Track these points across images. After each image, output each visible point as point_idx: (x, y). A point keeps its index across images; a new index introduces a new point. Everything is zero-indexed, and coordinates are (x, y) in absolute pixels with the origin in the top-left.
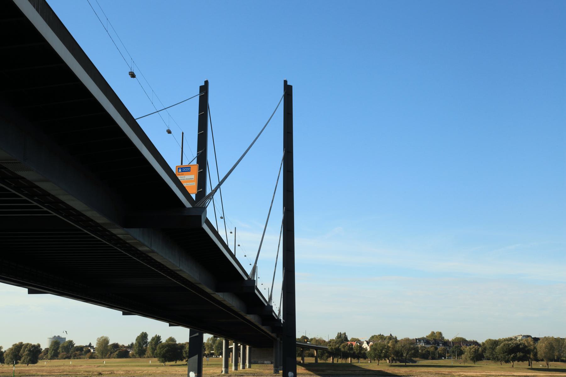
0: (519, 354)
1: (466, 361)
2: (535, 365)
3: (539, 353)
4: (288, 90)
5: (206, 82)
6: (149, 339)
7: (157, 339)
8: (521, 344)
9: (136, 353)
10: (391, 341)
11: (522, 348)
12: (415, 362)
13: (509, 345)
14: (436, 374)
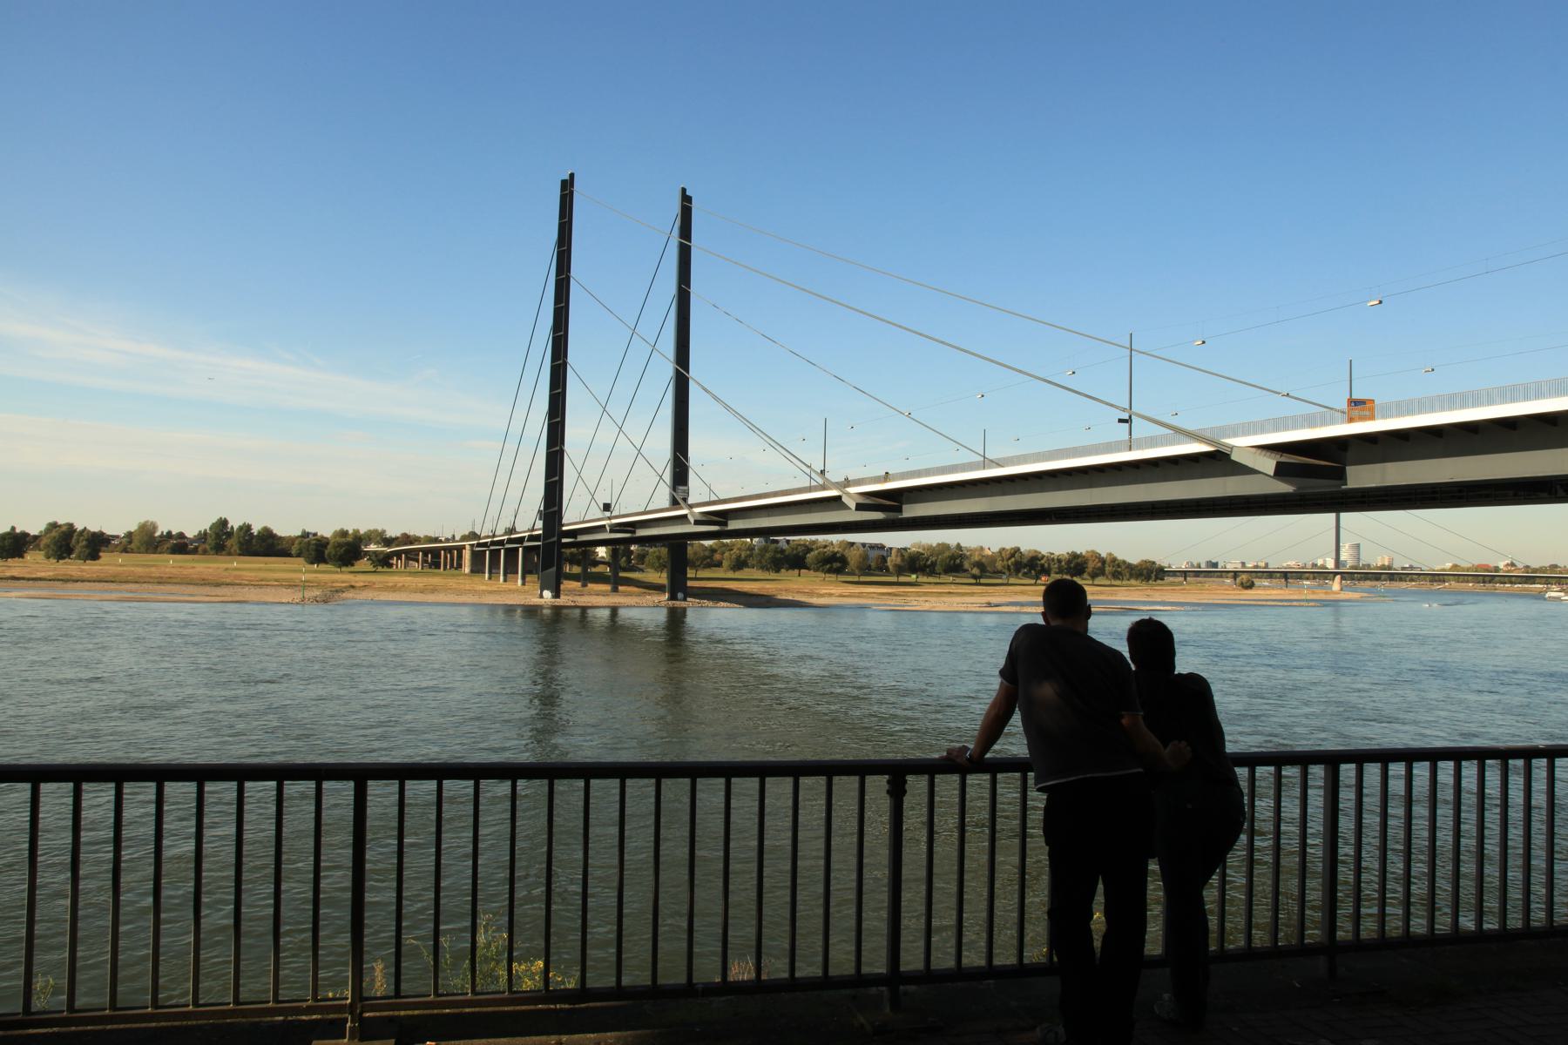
4: (686, 199)
5: (572, 176)
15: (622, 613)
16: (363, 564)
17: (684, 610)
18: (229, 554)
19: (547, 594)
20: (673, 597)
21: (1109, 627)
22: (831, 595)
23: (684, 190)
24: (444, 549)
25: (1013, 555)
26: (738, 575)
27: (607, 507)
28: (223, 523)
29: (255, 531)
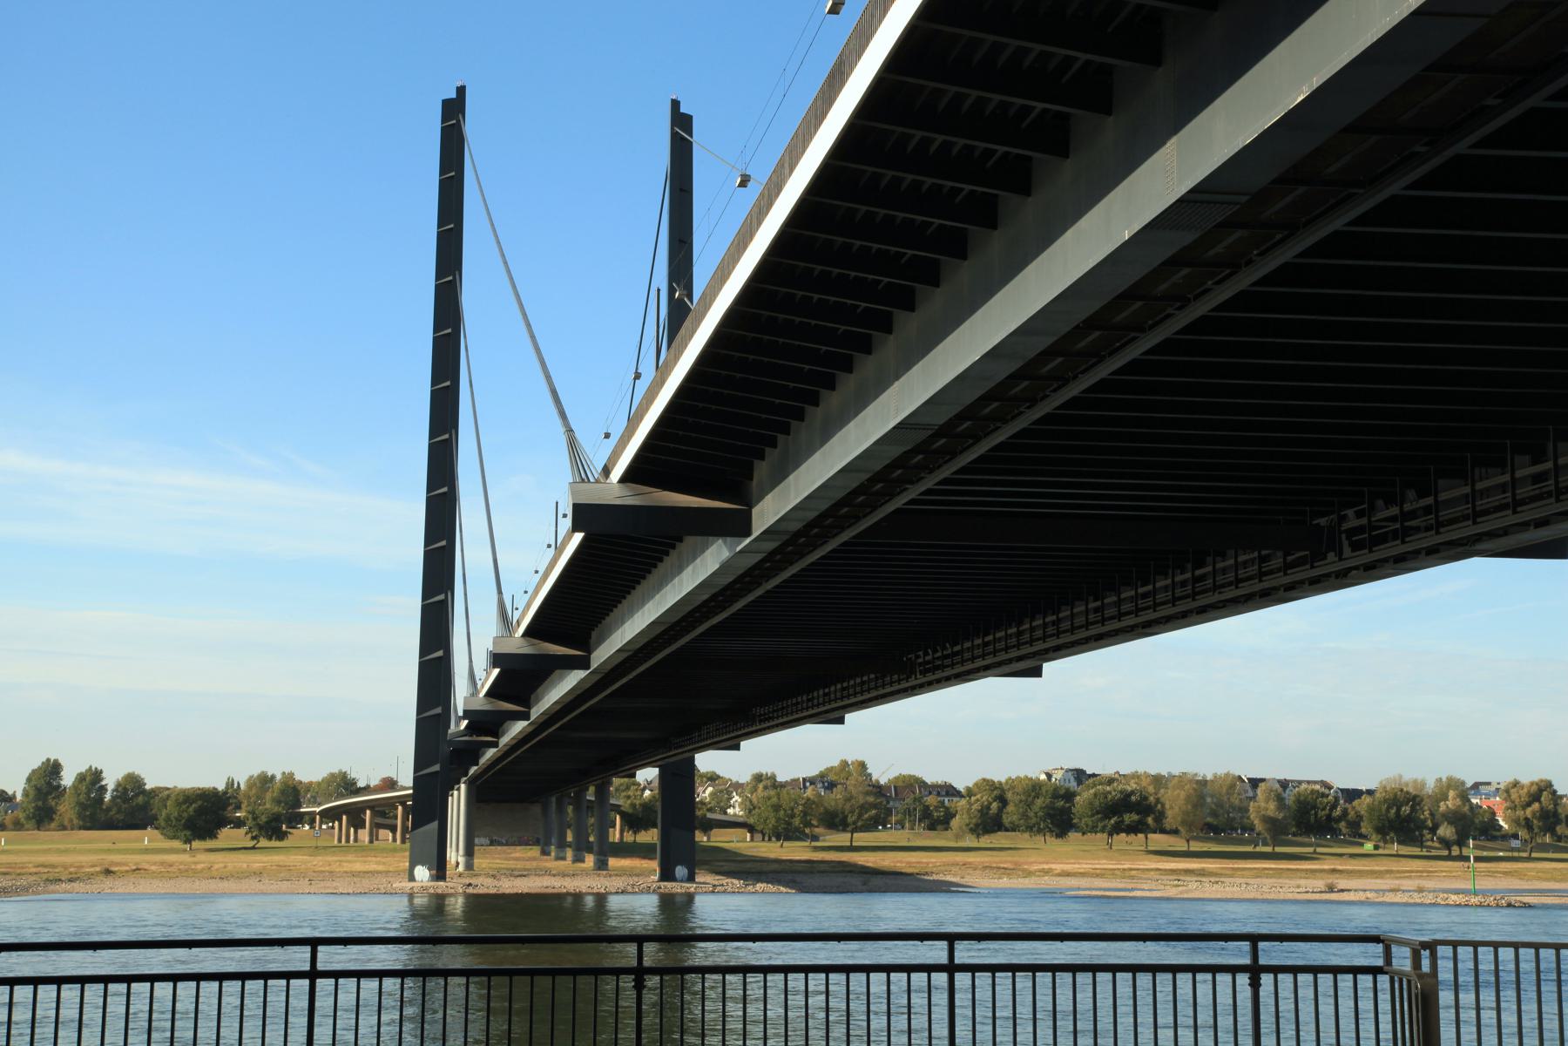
0: (1131, 818)
1: (958, 837)
2: (1158, 840)
3: (1169, 813)
4: (681, 122)
5: (461, 91)
6: (68, 779)
7: (93, 778)
8: (1132, 793)
9: (28, 818)
10: (761, 786)
11: (1138, 803)
12: (815, 838)
13: (1106, 794)
14: (985, 868)
15: (614, 902)
16: (227, 835)
17: (690, 898)
18: (64, 828)
19: (422, 873)
20: (667, 875)
21: (590, 860)
22: (1046, 872)
23: (675, 104)
24: (371, 805)
25: (1535, 797)
26: (985, 841)
28: (52, 769)
29: (110, 781)
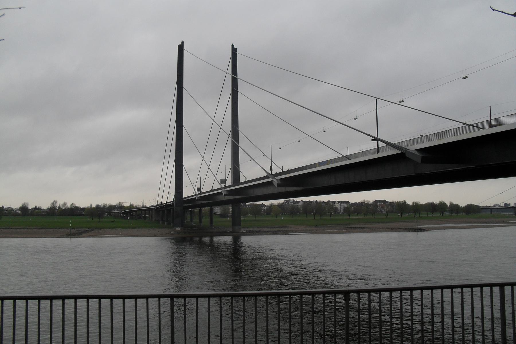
4: (234, 51)
5: (183, 43)
23: (233, 46)
27: (199, 189)
